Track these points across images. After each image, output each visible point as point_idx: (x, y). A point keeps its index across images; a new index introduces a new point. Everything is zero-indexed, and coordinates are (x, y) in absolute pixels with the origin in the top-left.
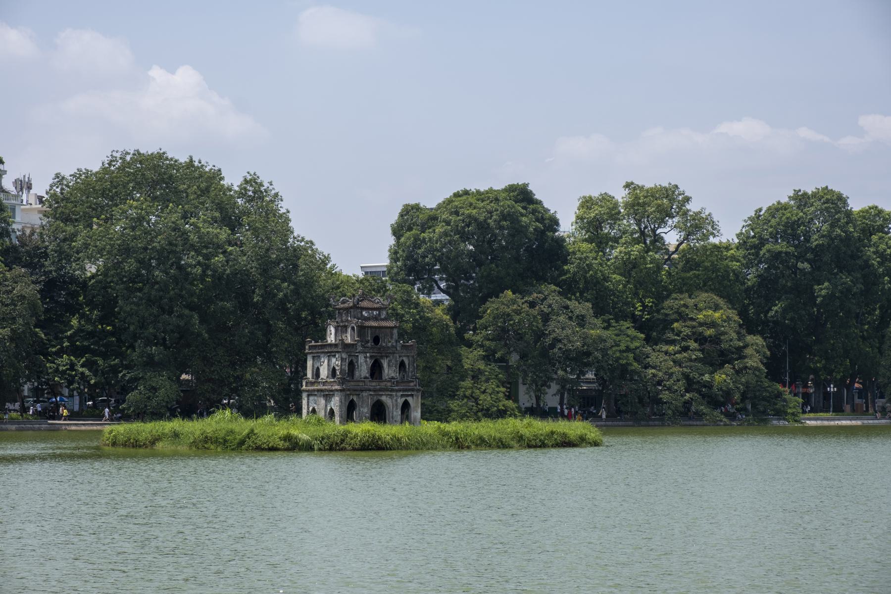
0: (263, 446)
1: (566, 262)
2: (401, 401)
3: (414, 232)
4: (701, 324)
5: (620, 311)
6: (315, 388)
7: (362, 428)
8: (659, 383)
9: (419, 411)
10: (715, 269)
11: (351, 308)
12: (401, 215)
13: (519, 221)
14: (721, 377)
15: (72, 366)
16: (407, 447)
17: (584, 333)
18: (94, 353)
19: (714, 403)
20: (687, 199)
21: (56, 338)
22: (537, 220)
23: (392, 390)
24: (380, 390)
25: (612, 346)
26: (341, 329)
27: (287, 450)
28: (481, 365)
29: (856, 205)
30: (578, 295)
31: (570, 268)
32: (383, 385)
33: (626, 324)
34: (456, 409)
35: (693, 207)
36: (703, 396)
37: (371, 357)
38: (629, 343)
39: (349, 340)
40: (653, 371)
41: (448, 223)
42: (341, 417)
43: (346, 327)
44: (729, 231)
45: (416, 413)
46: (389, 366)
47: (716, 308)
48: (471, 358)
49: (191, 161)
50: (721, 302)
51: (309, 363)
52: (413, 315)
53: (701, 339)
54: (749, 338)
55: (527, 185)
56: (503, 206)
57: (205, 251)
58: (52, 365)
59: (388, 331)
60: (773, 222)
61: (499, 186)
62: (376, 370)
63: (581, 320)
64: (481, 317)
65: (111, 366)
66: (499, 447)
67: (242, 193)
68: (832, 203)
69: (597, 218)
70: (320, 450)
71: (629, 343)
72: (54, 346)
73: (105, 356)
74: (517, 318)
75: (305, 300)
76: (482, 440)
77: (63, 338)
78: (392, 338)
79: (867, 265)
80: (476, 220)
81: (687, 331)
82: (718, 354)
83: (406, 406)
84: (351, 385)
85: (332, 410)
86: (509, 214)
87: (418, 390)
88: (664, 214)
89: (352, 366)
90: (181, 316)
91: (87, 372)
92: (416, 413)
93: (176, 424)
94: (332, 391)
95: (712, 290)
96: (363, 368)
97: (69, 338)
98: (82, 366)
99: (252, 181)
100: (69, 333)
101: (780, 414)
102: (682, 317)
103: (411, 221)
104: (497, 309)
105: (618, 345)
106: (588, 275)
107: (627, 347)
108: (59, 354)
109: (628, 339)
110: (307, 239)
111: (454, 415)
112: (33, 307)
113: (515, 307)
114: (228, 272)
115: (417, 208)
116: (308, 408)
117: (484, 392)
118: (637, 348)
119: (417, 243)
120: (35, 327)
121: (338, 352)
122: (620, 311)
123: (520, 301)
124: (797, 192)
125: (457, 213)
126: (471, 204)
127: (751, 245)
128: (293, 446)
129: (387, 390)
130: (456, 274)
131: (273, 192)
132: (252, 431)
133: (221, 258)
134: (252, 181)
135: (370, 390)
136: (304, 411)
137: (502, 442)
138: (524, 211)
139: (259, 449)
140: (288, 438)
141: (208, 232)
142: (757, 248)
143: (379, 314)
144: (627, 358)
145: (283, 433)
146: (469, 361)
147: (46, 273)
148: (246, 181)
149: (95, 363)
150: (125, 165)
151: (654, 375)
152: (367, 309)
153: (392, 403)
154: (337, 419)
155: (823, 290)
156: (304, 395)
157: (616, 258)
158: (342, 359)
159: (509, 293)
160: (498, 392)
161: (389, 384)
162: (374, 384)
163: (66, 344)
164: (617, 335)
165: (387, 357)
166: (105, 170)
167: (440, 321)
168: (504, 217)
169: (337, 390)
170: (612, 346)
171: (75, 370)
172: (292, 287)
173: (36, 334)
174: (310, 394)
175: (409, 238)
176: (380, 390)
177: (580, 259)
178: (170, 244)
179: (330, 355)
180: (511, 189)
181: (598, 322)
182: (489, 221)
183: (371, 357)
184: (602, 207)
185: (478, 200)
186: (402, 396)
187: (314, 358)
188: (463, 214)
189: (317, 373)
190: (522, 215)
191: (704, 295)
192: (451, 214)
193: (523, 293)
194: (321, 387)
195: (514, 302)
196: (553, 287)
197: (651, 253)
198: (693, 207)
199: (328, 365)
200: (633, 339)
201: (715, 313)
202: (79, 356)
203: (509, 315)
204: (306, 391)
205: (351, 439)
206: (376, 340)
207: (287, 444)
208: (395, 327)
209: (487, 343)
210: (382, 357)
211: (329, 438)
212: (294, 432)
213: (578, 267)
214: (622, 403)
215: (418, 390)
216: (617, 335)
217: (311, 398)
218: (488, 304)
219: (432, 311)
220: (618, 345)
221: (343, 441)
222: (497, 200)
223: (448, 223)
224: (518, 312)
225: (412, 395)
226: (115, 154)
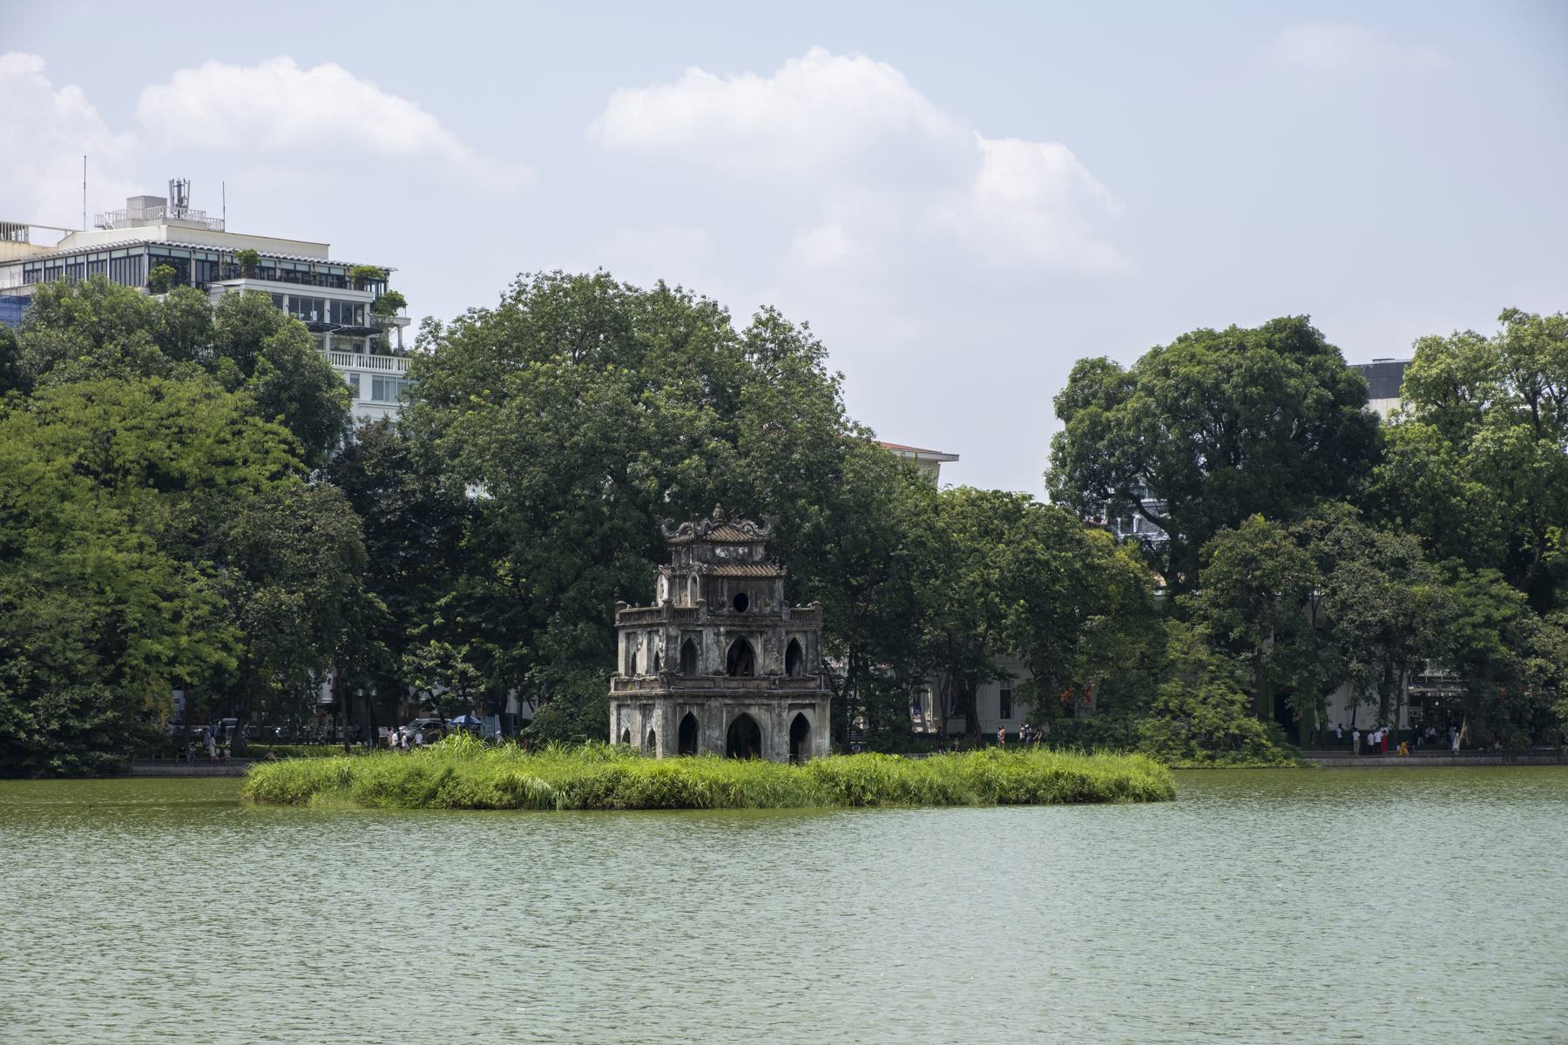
0: (463, 801)
1: (1381, 460)
2: (789, 717)
3: (1092, 409)
5: (1482, 550)
6: (628, 692)
7: (709, 768)
9: (827, 734)
11: (692, 542)
12: (1074, 380)
13: (1281, 386)
15: (445, 661)
16: (738, 803)
17: (1398, 592)
18: (488, 636)
21: (422, 610)
22: (1323, 384)
23: (771, 696)
24: (746, 695)
25: (1458, 616)
26: (677, 582)
27: (509, 807)
28: (1202, 653)
30: (1399, 520)
31: (1385, 471)
34: (1149, 734)
37: (728, 634)
38: (1492, 610)
39: (688, 602)
40: (1539, 661)
41: (1150, 391)
42: (666, 746)
43: (684, 577)
45: (822, 739)
46: (765, 649)
49: (663, 289)
51: (622, 646)
52: (1066, 561)
55: (1307, 318)
56: (1251, 359)
57: (665, 450)
58: (411, 658)
59: (764, 584)
62: (740, 659)
63: (1400, 566)
64: (1206, 565)
65: (513, 659)
66: (937, 804)
67: (754, 343)
70: (566, 808)
71: (1492, 610)
72: (417, 625)
74: (1269, 564)
75: (855, 537)
77: (431, 611)
78: (772, 598)
80: (1199, 385)
83: (800, 730)
84: (688, 686)
85: (652, 733)
86: (1262, 373)
87: (824, 696)
89: (690, 652)
90: (626, 567)
91: (471, 671)
92: (822, 739)
94: (651, 698)
96: (713, 652)
98: (466, 659)
99: (771, 321)
100: (443, 601)
103: (1091, 389)
104: (1231, 549)
105: (1472, 615)
106: (1417, 484)
107: (1488, 618)
108: (424, 639)
109: (1491, 601)
110: (863, 425)
111: (1143, 744)
113: (1267, 544)
114: (710, 486)
115: (1101, 364)
116: (619, 730)
117: (1204, 701)
118: (1507, 619)
119: (1097, 430)
120: (365, 592)
121: (661, 625)
122: (1482, 550)
123: (1279, 533)
125: (1166, 373)
126: (1193, 356)
128: (593, 801)
129: (759, 695)
131: (811, 341)
132: (450, 771)
134: (771, 321)
135: (724, 696)
136: (613, 736)
137: (945, 794)
138: (1295, 366)
139: (457, 805)
140: (510, 786)
141: (674, 416)
143: (750, 554)
144: (1487, 638)
145: (500, 774)
146: (1178, 646)
148: (759, 322)
149: (488, 655)
151: (1541, 669)
152: (724, 544)
153: (774, 722)
154: (659, 749)
156: (613, 705)
157: (1477, 450)
158: (669, 639)
159: (1260, 518)
160: (1232, 703)
161: (765, 684)
162: (733, 684)
163: (438, 620)
164: (1469, 595)
165: (762, 633)
166: (507, 312)
167: (1124, 571)
169: (658, 697)
170: (1458, 616)
171: (452, 667)
172: (827, 512)
173: (370, 603)
174: (622, 703)
175: (1082, 421)
176: (746, 695)
177: (1403, 454)
179: (651, 631)
180: (1279, 325)
181: (1434, 570)
182: (1225, 386)
183: (728, 634)
184: (1454, 356)
185: (1209, 348)
186: (791, 707)
187: (628, 636)
188: (1176, 375)
189: (632, 667)
190: (1291, 374)
192: (1158, 374)
194: (636, 691)
195: (1266, 534)
196: (1347, 506)
197: (1542, 441)
199: (649, 650)
200: (1501, 601)
202: (457, 642)
203: (1253, 559)
204: (616, 698)
205: (627, 787)
206: (740, 602)
207: (507, 797)
208: (779, 577)
209: (1215, 612)
210: (752, 634)
211: (582, 785)
212: (522, 776)
215: (824, 696)
216: (1469, 595)
217: (624, 712)
218: (1217, 540)
219: (1111, 554)
220: (1472, 615)
221: (609, 791)
222: (1242, 347)
223: (1150, 391)
224: (1270, 553)
225: (812, 706)
226: (523, 280)
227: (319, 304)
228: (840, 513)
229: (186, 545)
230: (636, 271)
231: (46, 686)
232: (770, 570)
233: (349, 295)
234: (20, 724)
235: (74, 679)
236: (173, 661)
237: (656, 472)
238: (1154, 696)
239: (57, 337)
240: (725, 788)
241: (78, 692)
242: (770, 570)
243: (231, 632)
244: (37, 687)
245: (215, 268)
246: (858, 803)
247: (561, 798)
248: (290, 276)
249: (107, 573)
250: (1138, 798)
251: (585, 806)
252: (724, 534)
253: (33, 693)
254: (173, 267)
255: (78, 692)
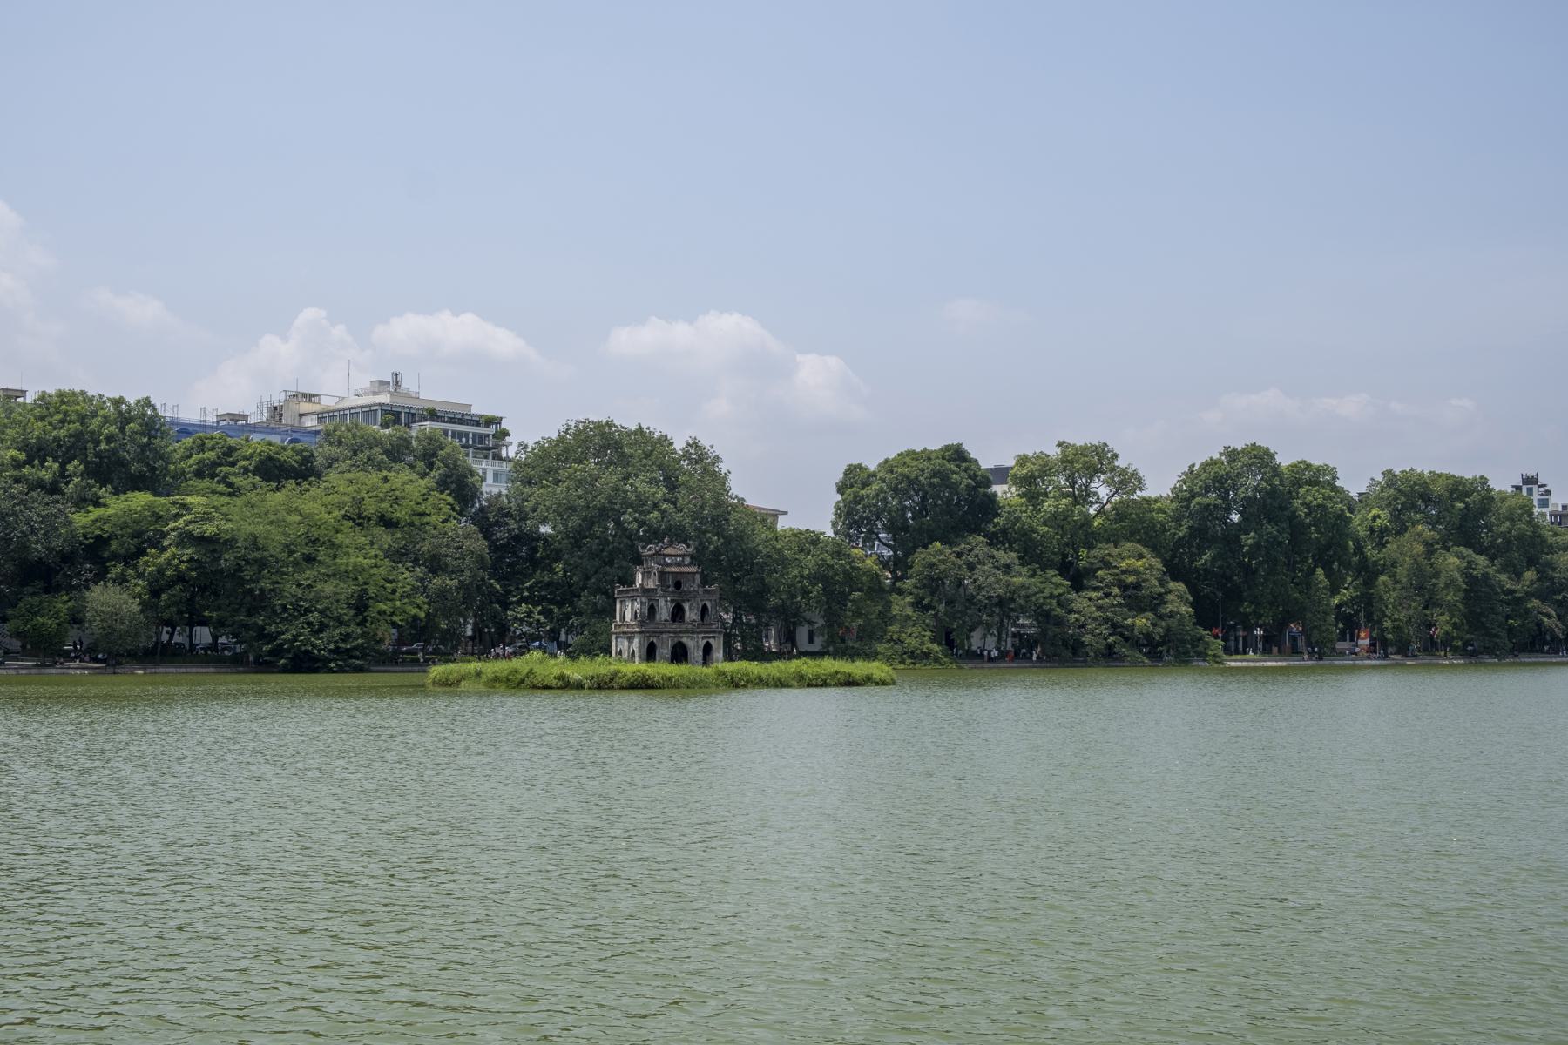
1: (998, 515)
2: (702, 643)
4: (1124, 572)
7: (661, 669)
8: (1083, 626)
10: (1142, 521)
14: (1141, 622)
15: (529, 614)
16: (676, 686)
18: (551, 602)
19: (1137, 645)
20: (1116, 456)
26: (646, 575)
28: (909, 611)
29: (1284, 460)
32: (684, 627)
33: (1051, 572)
35: (1120, 463)
36: (1127, 639)
39: (651, 585)
44: (1159, 484)
45: (718, 653)
47: (1141, 556)
48: (901, 605)
50: (1145, 551)
53: (1124, 587)
54: (1172, 585)
60: (1204, 476)
61: (935, 446)
62: (677, 614)
63: (1007, 568)
67: (686, 455)
68: (1260, 457)
69: (1031, 477)
73: (560, 605)
76: (760, 678)
79: (1293, 516)
81: (1109, 578)
82: (1135, 596)
83: (708, 649)
84: (651, 628)
88: (1093, 471)
89: (652, 610)
92: (718, 653)
93: (473, 666)
95: (1139, 542)
96: (664, 610)
97: (529, 589)
101: (1202, 655)
102: (1107, 565)
103: (854, 479)
108: (519, 603)
112: (481, 560)
115: (859, 467)
119: (857, 500)
124: (1226, 448)
127: (1183, 498)
130: (897, 528)
133: (656, 514)
140: (562, 677)
142: (1188, 500)
147: (509, 531)
149: (551, 611)
150: (578, 433)
153: (694, 645)
155: (1248, 539)
167: (870, 570)
168: (934, 475)
178: (610, 502)
179: (633, 599)
180: (947, 448)
181: (1024, 570)
191: (1129, 545)
193: (951, 544)
195: (941, 552)
198: (1120, 463)
200: (1057, 586)
201: (1138, 562)
202: (535, 604)
206: (678, 585)
213: (1007, 519)
214: (1052, 647)
224: (943, 562)
227: (467, 435)
228: (728, 540)
229: (398, 556)
230: (627, 419)
231: (328, 626)
232: (693, 569)
233: (482, 430)
234: (314, 646)
235: (341, 623)
236: (392, 614)
237: (636, 520)
238: (885, 632)
239: (334, 451)
240: (670, 679)
241: (344, 630)
242: (693, 569)
243: (420, 599)
244: (323, 627)
245: (414, 417)
246: (737, 686)
247: (587, 683)
248: (452, 421)
249: (359, 569)
250: (877, 684)
251: (599, 687)
252: (669, 551)
253: (321, 630)
254: (393, 416)
255: (344, 630)
